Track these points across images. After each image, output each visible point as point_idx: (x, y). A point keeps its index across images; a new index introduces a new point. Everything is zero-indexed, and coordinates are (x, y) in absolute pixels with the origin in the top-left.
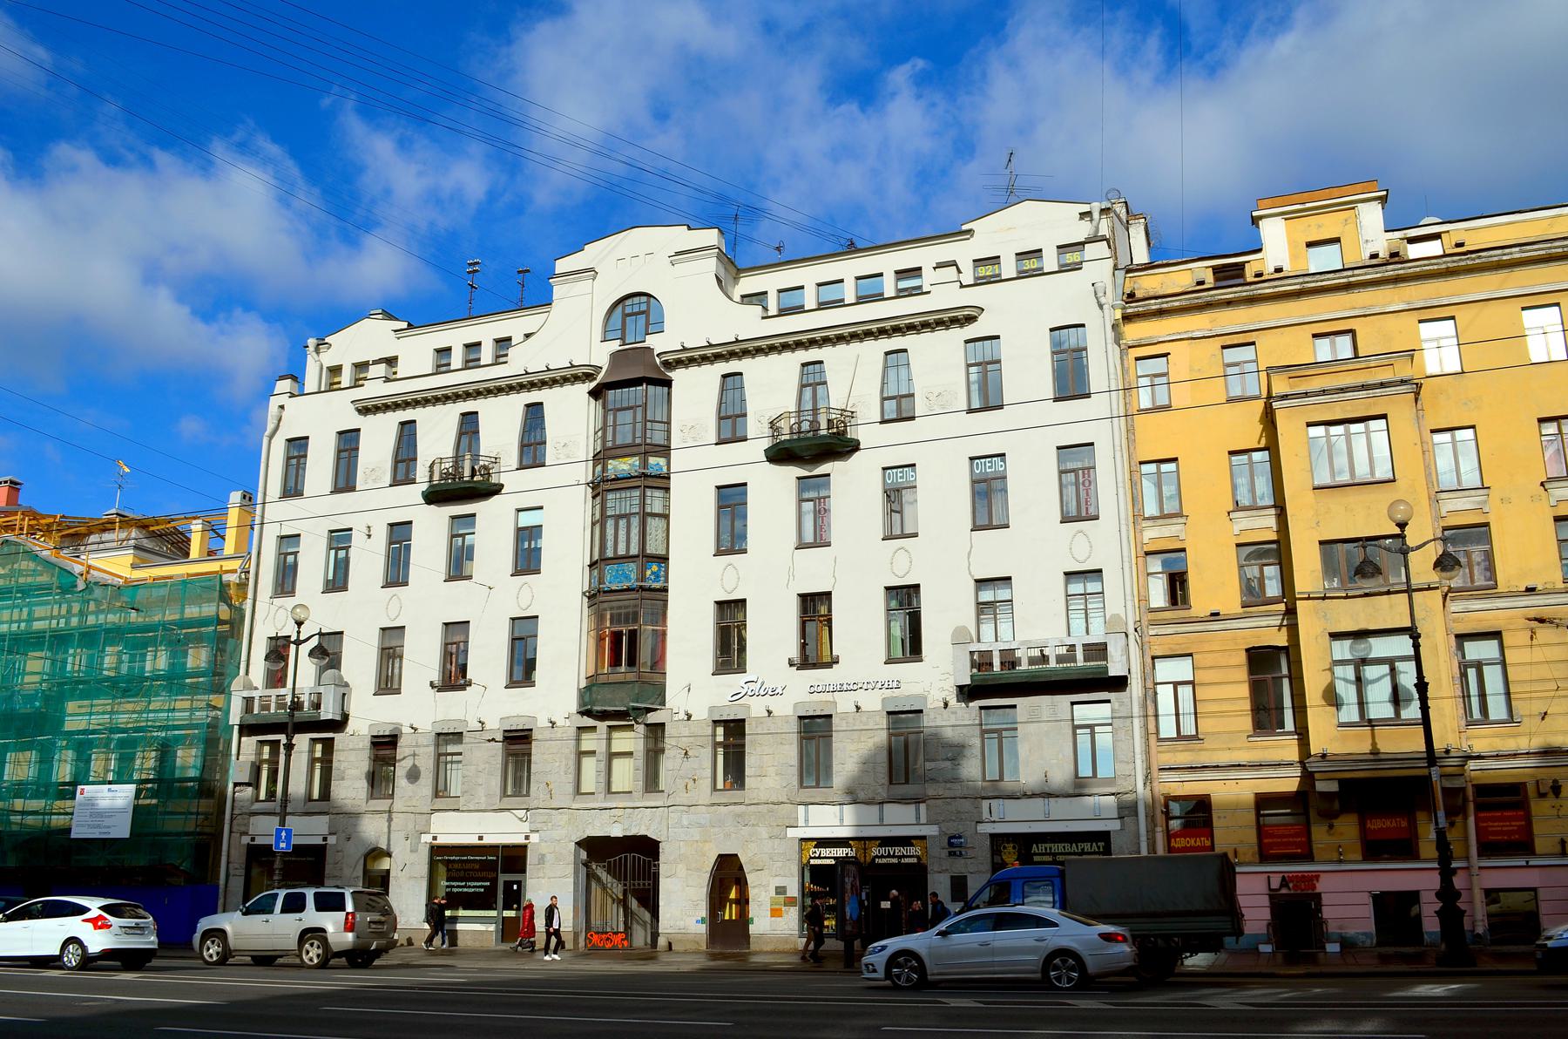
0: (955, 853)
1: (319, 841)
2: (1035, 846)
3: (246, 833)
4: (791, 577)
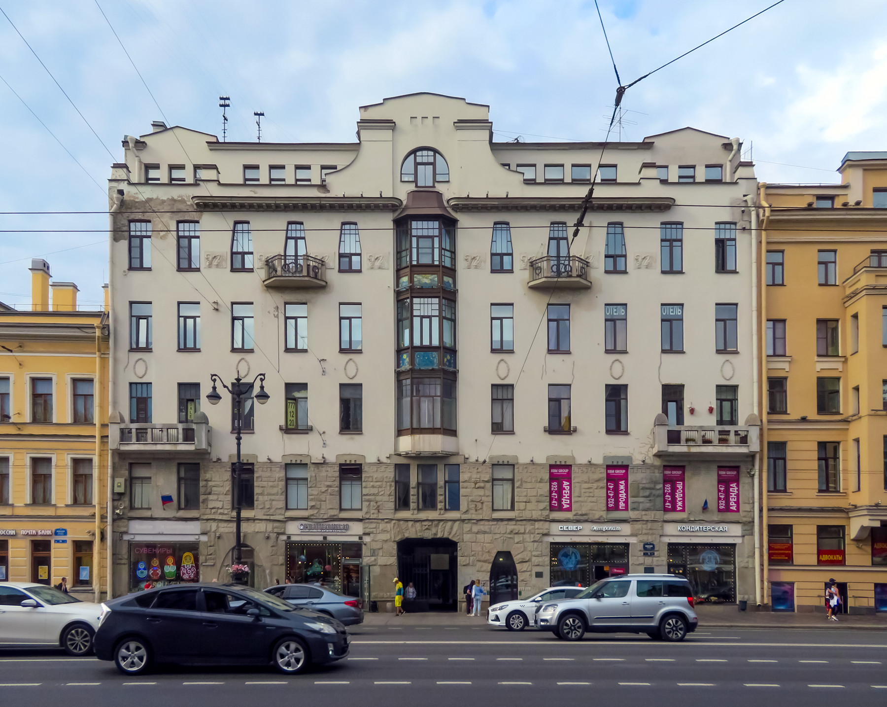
0: (647, 554)
1: (356, 539)
3: (283, 533)
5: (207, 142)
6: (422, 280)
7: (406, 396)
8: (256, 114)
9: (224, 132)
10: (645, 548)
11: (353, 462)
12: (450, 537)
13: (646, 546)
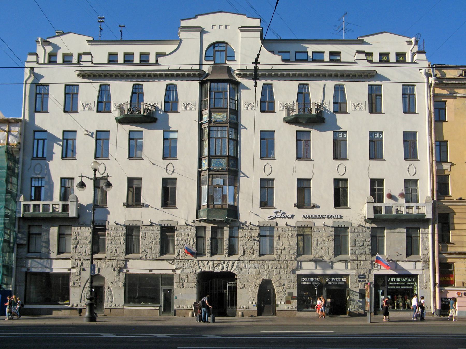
0: (361, 281)
1: (66, 271)
2: (389, 279)
3: (25, 267)
4: (294, 171)
5: (87, 41)
6: (216, 117)
7: (205, 184)
8: (120, 26)
9: (100, 36)
10: (359, 278)
11: (169, 225)
12: (232, 271)
13: (360, 276)
